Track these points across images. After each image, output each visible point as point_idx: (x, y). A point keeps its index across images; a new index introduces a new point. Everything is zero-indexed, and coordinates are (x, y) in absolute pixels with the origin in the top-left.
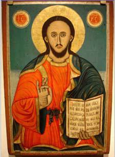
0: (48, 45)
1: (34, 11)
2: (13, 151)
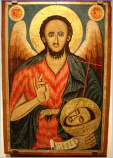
0: (46, 44)
1: (31, 12)
2: (9, 150)
